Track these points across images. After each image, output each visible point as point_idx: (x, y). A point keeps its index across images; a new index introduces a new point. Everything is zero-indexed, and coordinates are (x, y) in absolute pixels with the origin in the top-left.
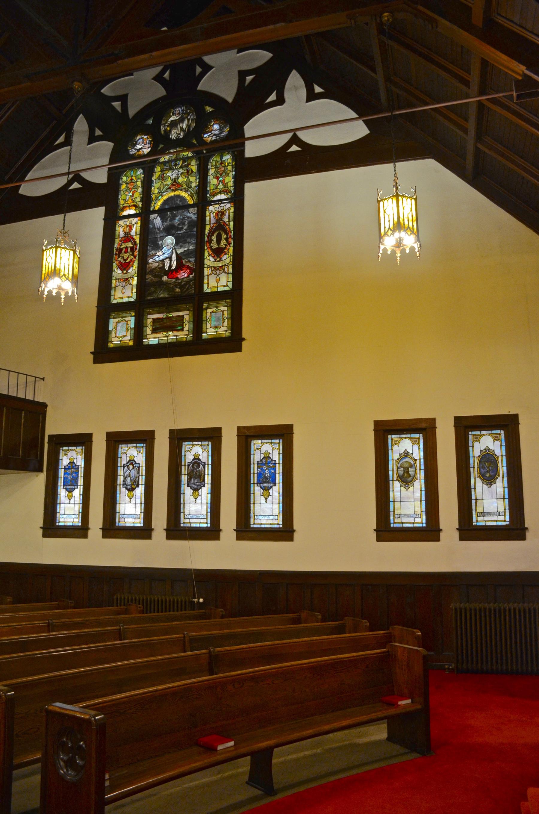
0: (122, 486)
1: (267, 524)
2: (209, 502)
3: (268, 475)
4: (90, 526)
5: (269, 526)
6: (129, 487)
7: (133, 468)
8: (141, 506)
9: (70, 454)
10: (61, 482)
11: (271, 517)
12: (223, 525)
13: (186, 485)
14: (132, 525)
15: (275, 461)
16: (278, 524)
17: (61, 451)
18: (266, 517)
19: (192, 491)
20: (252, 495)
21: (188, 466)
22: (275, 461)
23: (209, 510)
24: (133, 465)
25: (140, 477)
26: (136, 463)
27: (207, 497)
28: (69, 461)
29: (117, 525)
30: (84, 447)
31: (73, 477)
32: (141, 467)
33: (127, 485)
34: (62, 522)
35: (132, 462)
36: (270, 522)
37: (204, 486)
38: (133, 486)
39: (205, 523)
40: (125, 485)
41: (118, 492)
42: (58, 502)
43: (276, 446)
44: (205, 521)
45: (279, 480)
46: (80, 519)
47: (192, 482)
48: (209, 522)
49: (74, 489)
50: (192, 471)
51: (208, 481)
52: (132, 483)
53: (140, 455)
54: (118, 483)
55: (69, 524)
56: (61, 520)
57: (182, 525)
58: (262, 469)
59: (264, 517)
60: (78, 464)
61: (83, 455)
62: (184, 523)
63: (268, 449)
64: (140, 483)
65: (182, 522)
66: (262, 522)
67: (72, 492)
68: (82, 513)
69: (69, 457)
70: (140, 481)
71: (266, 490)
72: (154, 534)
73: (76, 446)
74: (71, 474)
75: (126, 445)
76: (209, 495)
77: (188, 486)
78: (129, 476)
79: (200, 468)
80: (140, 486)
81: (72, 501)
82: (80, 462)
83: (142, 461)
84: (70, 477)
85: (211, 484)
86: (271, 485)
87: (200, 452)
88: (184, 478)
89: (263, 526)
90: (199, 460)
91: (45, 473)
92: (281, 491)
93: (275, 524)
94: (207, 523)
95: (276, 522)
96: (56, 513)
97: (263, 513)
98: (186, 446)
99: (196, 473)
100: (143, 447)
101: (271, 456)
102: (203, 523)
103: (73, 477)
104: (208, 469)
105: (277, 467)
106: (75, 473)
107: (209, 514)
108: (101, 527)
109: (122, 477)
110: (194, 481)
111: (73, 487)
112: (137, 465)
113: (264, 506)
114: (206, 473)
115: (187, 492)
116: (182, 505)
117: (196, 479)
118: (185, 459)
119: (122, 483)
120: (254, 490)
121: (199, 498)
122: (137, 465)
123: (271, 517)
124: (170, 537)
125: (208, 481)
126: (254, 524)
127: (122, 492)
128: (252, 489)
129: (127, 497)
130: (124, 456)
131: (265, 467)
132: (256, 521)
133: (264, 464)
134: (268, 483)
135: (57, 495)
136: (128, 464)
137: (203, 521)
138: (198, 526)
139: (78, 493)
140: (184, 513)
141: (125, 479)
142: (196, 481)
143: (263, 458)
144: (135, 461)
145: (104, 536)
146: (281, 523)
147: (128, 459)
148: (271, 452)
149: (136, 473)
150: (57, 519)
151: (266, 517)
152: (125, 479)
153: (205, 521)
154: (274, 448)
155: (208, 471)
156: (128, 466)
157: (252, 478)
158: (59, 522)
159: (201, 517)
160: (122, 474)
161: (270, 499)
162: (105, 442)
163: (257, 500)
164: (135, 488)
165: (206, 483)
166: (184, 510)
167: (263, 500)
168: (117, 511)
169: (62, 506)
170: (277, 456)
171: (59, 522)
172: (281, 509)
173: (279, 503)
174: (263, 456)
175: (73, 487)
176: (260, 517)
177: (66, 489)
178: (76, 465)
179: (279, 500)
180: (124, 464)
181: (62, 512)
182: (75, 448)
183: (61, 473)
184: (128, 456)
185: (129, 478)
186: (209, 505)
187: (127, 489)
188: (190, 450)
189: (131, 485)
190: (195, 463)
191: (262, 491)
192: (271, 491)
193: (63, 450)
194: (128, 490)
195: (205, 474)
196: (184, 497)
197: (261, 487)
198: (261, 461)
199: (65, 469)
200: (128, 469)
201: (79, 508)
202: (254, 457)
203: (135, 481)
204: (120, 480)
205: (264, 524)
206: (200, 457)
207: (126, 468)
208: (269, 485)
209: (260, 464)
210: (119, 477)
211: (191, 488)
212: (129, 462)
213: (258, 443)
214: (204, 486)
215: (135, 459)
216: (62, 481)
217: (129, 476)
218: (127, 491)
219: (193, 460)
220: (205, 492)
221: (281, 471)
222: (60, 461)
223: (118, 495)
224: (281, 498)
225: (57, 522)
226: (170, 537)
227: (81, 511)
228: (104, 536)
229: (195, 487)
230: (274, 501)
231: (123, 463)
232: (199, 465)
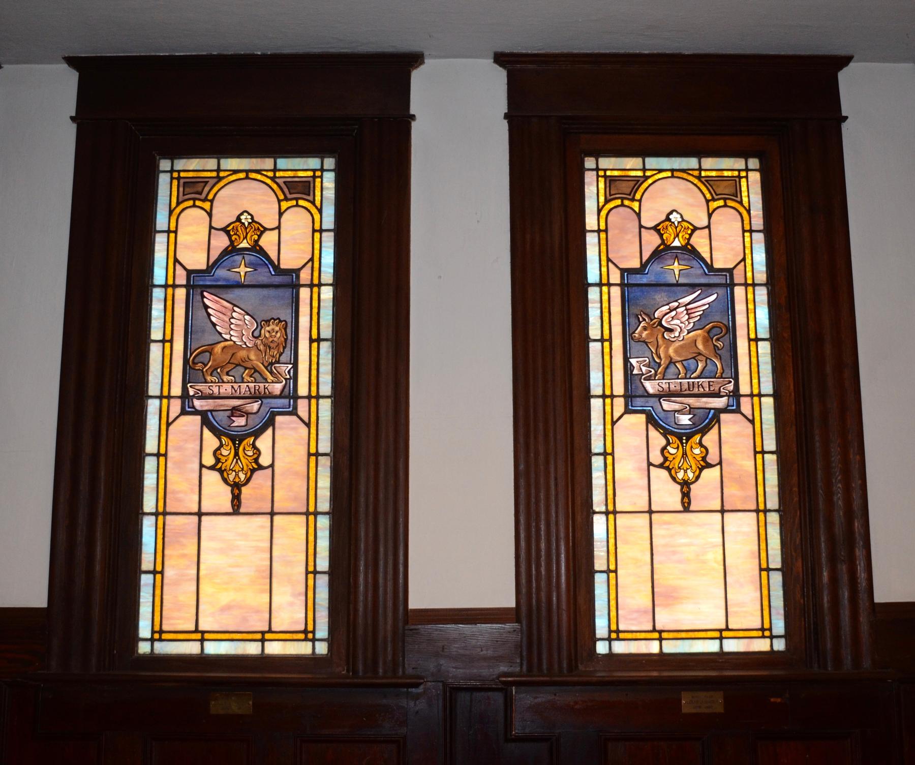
82: (303, 238)
169: (633, 528)
209: (636, 288)
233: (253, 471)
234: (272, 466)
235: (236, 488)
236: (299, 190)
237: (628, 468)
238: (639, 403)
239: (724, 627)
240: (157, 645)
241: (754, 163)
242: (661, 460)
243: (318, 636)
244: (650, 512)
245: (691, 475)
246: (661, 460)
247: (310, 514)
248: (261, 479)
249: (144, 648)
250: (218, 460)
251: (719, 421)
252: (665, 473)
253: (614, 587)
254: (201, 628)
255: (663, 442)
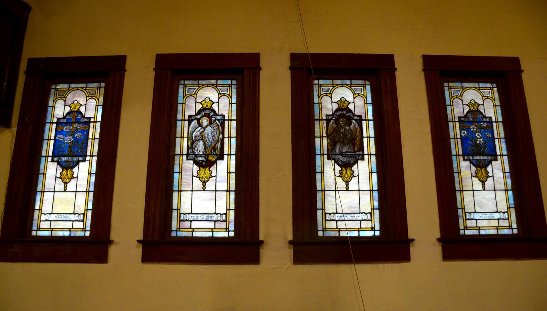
0: (185, 157)
1: (489, 228)
2: (375, 187)
3: (480, 141)
4: (113, 236)
5: (493, 232)
6: (200, 159)
7: (210, 123)
8: (323, 184)
9: (70, 98)
10: (49, 148)
11: (497, 216)
12: (413, 231)
13: (326, 156)
14: (209, 234)
15: (490, 118)
16: (510, 227)
17: (53, 91)
18: (487, 216)
19: (338, 168)
20: (456, 175)
21: (328, 121)
22: (490, 118)
23: (376, 204)
24: (210, 118)
25: (226, 140)
26: (216, 114)
27: (371, 179)
28: (68, 109)
29: (174, 234)
30: (103, 85)
31: (75, 139)
32: (226, 123)
33: (197, 156)
34: (44, 229)
35: (207, 112)
36: (495, 223)
37: (363, 159)
38: (210, 158)
39: (370, 228)
40: (191, 154)
41: (176, 169)
42: (39, 188)
43: (487, 93)
44: (369, 224)
45: (501, 150)
46: (89, 222)
47: (337, 151)
48: (377, 227)
49: (77, 163)
50: (336, 131)
51: (369, 149)
52: (208, 152)
53: (225, 101)
54: (178, 151)
55: (60, 234)
56: (44, 225)
57: (320, 234)
58: (468, 130)
59: (483, 216)
60: (90, 114)
61: (101, 99)
62: (325, 229)
63: (477, 98)
64: (226, 152)
65: (320, 227)
66: (481, 224)
67: (72, 168)
68: (93, 210)
69: (69, 102)
70: (226, 148)
71: (481, 168)
72: (265, 253)
73: (87, 82)
74: (72, 133)
75: (196, 82)
76: (375, 176)
77: (329, 159)
78: (201, 137)
79: (352, 126)
80: (226, 157)
81: (71, 186)
82: (92, 109)
83: (230, 111)
84: (68, 139)
85: (377, 155)
86: (489, 158)
87: (350, 98)
88: (321, 144)
89: (483, 232)
90: (350, 111)
91: (15, 129)
92: (507, 169)
93: (504, 228)
94: (373, 229)
95: (505, 223)
96: (34, 209)
97: (481, 207)
98: (320, 85)
99: (344, 135)
100: (230, 86)
101: (481, 108)
102: (366, 229)
103: (75, 139)
104: (368, 127)
105: (495, 128)
106: (82, 132)
107: (377, 212)
108: (141, 237)
109: (185, 140)
110: (341, 148)
111: (75, 159)
112: (218, 118)
113: (481, 196)
114: (365, 135)
115: (329, 172)
116: (319, 195)
117: (345, 145)
118: (320, 110)
119: (185, 152)
120: (459, 167)
121: (354, 181)
122: (218, 118)
123: (497, 216)
124: (300, 257)
125: (369, 149)
126: (466, 228)
127: (186, 171)
128: (455, 165)
129: (196, 180)
130: (190, 102)
131: (473, 128)
132: (469, 223)
133: (473, 123)
134: (483, 155)
135: (38, 174)
136: (199, 117)
137: (364, 224)
138: (355, 234)
139: (85, 171)
140: (323, 209)
141: (193, 143)
142: (345, 149)
143: (468, 112)
144: (214, 111)
145: (147, 258)
146: (514, 225)
147: (199, 106)
148: (480, 102)
149: (215, 133)
150: (35, 223)
151: (487, 216)
152: (193, 143)
153: (369, 224)
154: (484, 98)
155: (368, 132)
156: (198, 120)
157: (453, 146)
158: (39, 229)
159: (361, 217)
160: (186, 135)
161: (489, 183)
162: (153, 73)
163: (467, 185)
164: (215, 162)
165: (366, 152)
166: (323, 203)
167: (477, 185)
168: (175, 206)
169: (48, 196)
170: (491, 110)
171: (39, 229)
172: (512, 202)
173: (506, 190)
174: (467, 109)
175: (75, 159)
176: (477, 216)
177: (59, 163)
178: (83, 117)
179: (506, 184)
180: (190, 116)
181: (46, 208)
182: (84, 85)
183: (50, 132)
184: (199, 100)
185: (201, 143)
186: (376, 194)
187: (196, 162)
188: (330, 94)
189: (207, 155)
190: (341, 116)
191: (474, 169)
192: (489, 169)
193: (56, 90)
194: (199, 164)
195: (362, 137)
196: (323, 179)
197: (471, 162)
198: (466, 116)
199: (58, 123)
200: (200, 124)
201: (87, 201)
202: (452, 110)
203: (214, 149)
204: (182, 145)
205: (485, 228)
206: (351, 107)
207: (194, 123)
208: (485, 158)
209: (464, 122)
210: (178, 140)
211: (336, 162)
212: (200, 112)
213: (455, 88)
214: (363, 159)
215: (215, 107)
216: (51, 147)
217: (201, 137)
218: (196, 168)
219: (337, 110)
220: (365, 171)
221: (502, 135)
222: (50, 109)
223: (176, 176)
224: (509, 181)
225: (35, 228)
226: (300, 257)
227: (90, 206)
228: (147, 258)
229: (345, 159)
230: (498, 186)
231: (187, 114)
232: (349, 120)
233: (210, 178)
234: (77, 177)
235: (204, 183)
236: (91, 96)
237: (186, 177)
238: (190, 157)
239: (213, 227)
240: (179, 233)
241: (495, 85)
242: (197, 174)
243: (87, 229)
244: (216, 191)
245: (68, 180)
246: (339, 174)
247: (228, 191)
248: (73, 181)
249: (377, 233)
250: (61, 175)
251: (216, 163)
252: (60, 180)
253: (60, 216)
254: (192, 227)
255: (198, 169)
